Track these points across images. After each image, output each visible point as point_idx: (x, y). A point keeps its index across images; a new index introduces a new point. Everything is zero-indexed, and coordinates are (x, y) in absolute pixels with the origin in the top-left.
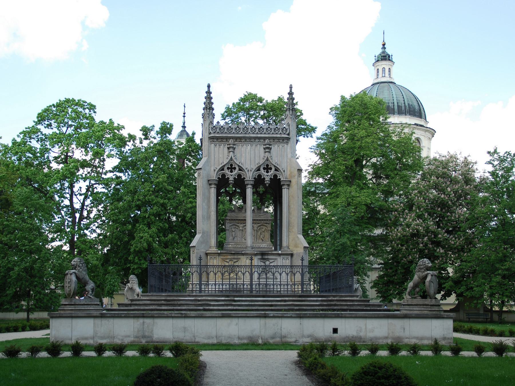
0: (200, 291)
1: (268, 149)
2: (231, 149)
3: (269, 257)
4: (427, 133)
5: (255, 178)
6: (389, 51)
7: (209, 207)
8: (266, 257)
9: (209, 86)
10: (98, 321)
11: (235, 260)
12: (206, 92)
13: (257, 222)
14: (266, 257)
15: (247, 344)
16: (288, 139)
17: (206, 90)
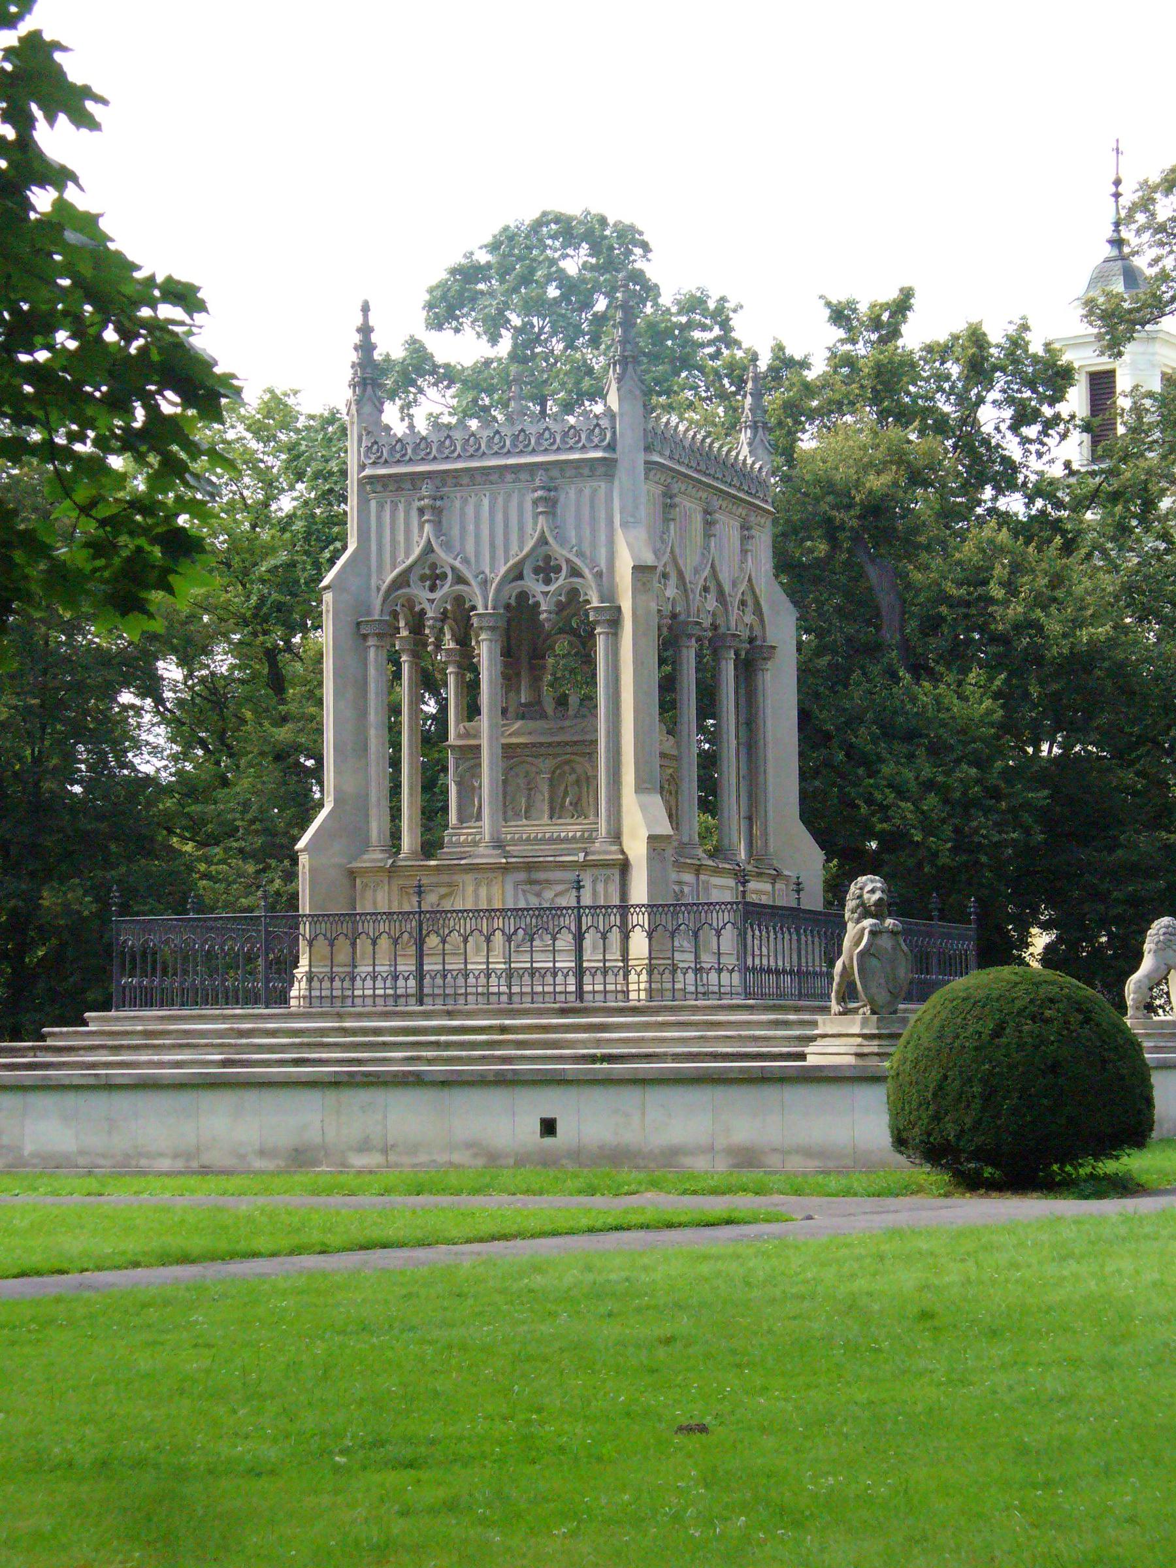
0: (580, 993)
1: (550, 505)
2: (436, 513)
3: (550, 875)
5: (508, 607)
7: (363, 713)
8: (541, 876)
9: (366, 309)
11: (443, 890)
12: (359, 330)
13: (551, 751)
14: (541, 876)
17: (359, 321)
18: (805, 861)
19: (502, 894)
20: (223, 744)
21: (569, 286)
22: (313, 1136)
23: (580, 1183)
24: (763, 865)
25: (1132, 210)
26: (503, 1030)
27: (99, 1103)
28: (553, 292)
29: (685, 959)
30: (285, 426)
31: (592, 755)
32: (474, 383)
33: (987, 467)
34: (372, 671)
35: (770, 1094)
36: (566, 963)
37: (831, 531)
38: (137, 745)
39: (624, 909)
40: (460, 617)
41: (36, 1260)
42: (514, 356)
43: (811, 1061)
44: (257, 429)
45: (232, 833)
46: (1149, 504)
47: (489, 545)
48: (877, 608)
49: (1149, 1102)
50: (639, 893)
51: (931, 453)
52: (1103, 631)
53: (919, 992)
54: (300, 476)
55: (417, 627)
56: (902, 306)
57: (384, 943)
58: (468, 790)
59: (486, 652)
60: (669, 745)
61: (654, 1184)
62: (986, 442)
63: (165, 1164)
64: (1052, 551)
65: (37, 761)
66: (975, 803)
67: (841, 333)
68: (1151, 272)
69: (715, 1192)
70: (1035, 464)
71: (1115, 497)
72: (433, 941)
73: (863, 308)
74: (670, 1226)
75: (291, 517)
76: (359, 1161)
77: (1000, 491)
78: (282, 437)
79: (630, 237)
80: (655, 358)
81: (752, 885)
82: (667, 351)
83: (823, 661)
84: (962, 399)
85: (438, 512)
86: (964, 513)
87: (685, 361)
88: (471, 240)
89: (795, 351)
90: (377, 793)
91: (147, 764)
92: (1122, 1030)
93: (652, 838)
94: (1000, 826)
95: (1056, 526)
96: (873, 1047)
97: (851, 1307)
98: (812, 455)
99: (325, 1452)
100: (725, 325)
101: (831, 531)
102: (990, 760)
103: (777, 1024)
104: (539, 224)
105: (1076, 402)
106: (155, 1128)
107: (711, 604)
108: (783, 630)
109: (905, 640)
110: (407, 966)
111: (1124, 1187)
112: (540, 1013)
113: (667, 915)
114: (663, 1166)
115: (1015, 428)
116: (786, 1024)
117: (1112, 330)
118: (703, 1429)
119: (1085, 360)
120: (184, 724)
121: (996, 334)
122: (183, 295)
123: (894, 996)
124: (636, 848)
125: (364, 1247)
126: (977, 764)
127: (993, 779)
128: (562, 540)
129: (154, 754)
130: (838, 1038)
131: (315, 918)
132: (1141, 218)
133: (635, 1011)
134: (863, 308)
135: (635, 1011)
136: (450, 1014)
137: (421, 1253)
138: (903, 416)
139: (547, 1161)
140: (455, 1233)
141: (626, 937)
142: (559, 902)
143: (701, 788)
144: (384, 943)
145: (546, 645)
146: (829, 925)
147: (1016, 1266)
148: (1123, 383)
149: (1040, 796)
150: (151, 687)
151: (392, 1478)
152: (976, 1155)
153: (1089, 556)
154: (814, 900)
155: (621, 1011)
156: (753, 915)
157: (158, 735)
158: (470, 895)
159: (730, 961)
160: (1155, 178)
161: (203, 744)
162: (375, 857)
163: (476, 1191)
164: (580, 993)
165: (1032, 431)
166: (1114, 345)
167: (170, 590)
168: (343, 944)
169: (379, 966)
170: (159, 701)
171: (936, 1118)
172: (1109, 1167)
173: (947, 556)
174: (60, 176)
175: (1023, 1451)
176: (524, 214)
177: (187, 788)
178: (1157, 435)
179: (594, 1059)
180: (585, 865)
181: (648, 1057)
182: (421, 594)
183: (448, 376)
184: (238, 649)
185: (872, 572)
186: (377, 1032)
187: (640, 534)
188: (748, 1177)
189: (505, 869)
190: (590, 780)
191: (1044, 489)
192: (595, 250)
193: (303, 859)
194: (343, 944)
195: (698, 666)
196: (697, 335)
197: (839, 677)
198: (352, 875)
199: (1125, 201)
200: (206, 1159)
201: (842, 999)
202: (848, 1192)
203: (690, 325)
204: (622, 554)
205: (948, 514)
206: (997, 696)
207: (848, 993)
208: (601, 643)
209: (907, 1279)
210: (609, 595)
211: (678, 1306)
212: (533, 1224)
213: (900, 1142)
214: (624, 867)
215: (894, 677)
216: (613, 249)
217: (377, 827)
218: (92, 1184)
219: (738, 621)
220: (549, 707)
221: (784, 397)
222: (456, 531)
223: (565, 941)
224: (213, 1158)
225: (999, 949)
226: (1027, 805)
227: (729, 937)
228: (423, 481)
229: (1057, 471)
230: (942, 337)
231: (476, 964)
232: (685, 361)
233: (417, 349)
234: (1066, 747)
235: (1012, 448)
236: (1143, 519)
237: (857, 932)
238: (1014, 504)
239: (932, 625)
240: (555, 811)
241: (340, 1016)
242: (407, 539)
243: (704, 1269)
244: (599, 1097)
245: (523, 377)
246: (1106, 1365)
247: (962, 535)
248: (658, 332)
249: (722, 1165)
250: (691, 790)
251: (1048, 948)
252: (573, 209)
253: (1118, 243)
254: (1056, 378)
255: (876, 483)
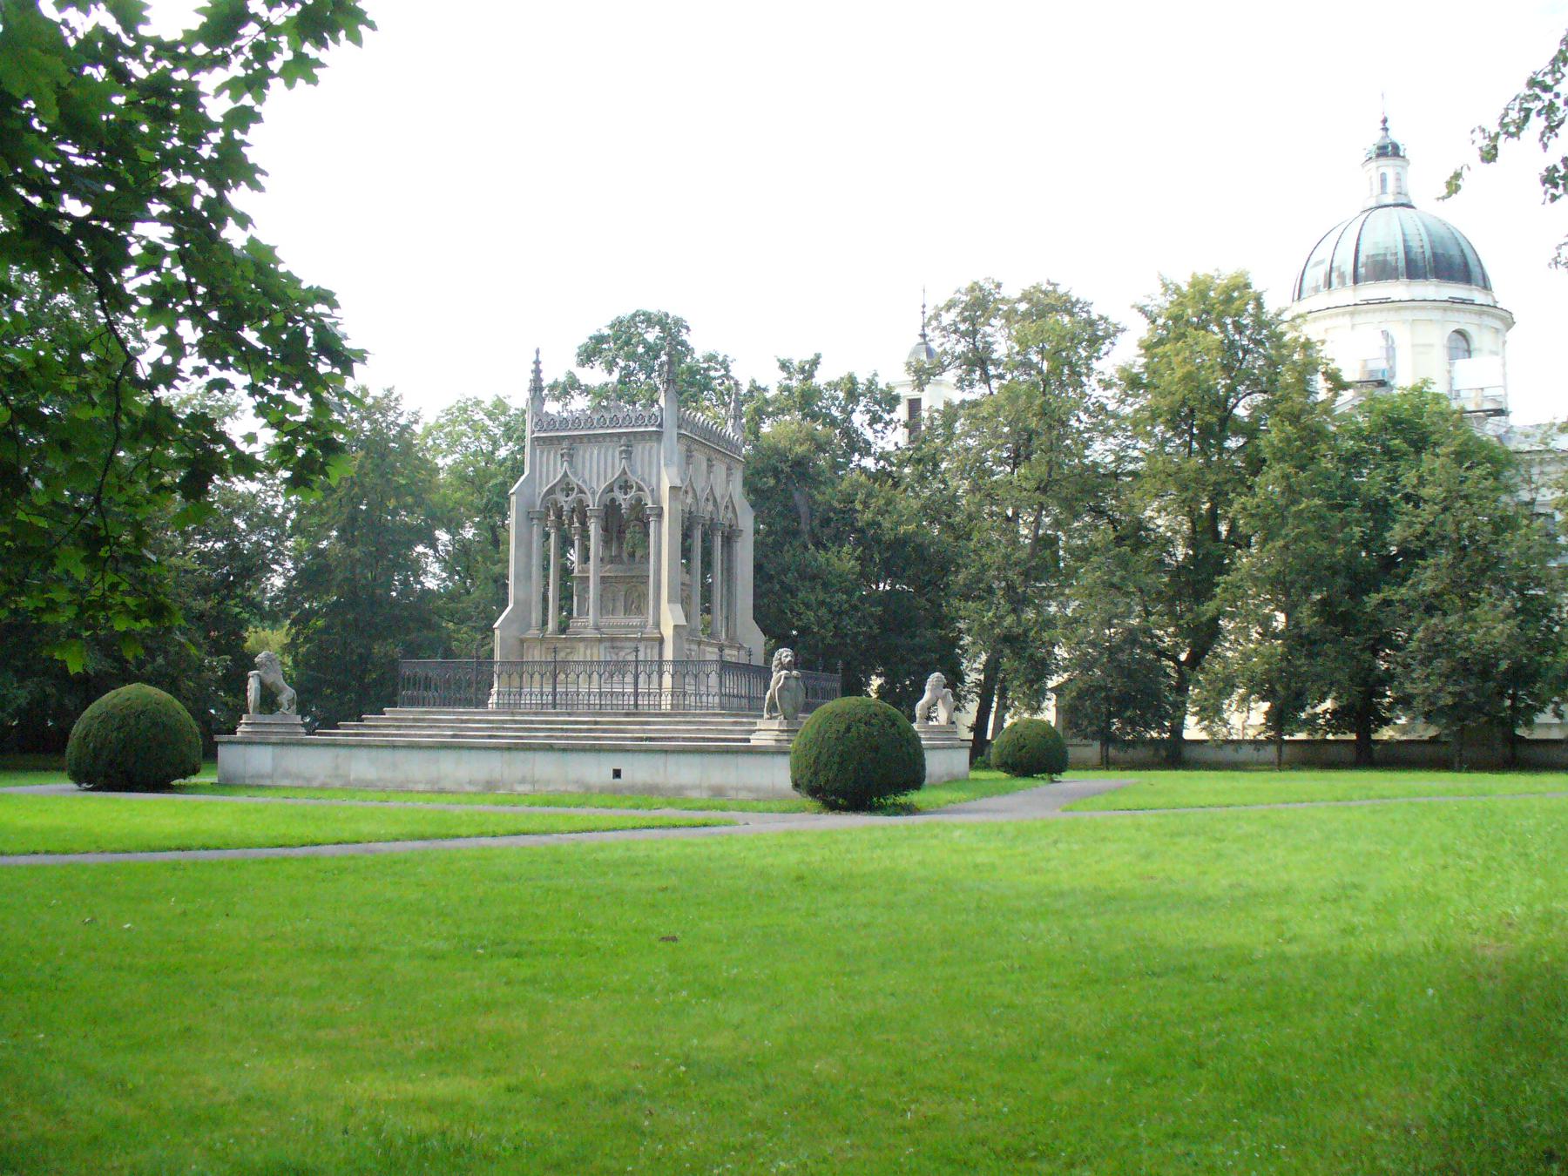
0: (636, 705)
1: (628, 454)
2: (570, 457)
4: (1485, 318)
6: (1395, 136)
7: (529, 557)
9: (538, 352)
10: (278, 750)
14: (618, 644)
15: (219, 784)
16: (659, 435)
18: (754, 639)
19: (599, 653)
20: (468, 572)
21: (649, 348)
22: (496, 775)
23: (628, 803)
24: (733, 642)
25: (930, 319)
26: (596, 723)
27: (386, 755)
28: (641, 350)
29: (690, 689)
30: (504, 413)
31: (646, 583)
32: (599, 393)
33: (857, 445)
34: (535, 538)
35: (730, 758)
36: (629, 689)
37: (776, 473)
38: (425, 573)
39: (661, 663)
40: (581, 511)
41: (346, 836)
42: (620, 381)
43: (753, 743)
44: (490, 415)
45: (470, 618)
46: (936, 465)
47: (596, 473)
48: (798, 513)
49: (923, 767)
50: (668, 654)
51: (828, 436)
52: (912, 527)
53: (808, 708)
54: (510, 439)
55: (559, 515)
56: (815, 363)
57: (537, 677)
58: (583, 600)
59: (593, 528)
60: (687, 578)
61: (671, 805)
62: (856, 431)
63: (421, 787)
64: (887, 487)
65: (374, 579)
66: (847, 613)
67: (785, 375)
68: (939, 350)
69: (701, 809)
70: (881, 443)
71: (919, 461)
72: (562, 677)
73: (796, 363)
74: (675, 826)
75: (505, 459)
76: (520, 788)
77: (862, 456)
78: (502, 419)
79: (679, 323)
80: (691, 385)
81: (727, 651)
82: (690, 381)
83: (770, 540)
84: (844, 410)
85: (571, 456)
86: (844, 466)
87: (706, 387)
88: (601, 324)
89: (761, 383)
90: (536, 598)
91: (431, 583)
92: (911, 730)
93: (676, 627)
94: (858, 625)
95: (890, 474)
96: (785, 736)
97: (762, 874)
98: (768, 435)
99: (471, 948)
100: (727, 369)
101: (776, 473)
102: (854, 590)
103: (735, 723)
104: (635, 316)
105: (901, 412)
106: (416, 767)
107: (710, 507)
108: (746, 521)
109: (812, 530)
110: (548, 689)
111: (909, 810)
112: (616, 715)
113: (683, 667)
114: (675, 796)
115: (870, 425)
116: (741, 724)
117: (919, 378)
118: (674, 939)
119: (906, 392)
120: (448, 566)
121: (862, 379)
122: (326, 297)
123: (796, 711)
124: (668, 632)
125: (516, 834)
126: (846, 592)
127: (854, 601)
128: (633, 472)
129: (433, 578)
130: (766, 731)
131: (502, 663)
132: (934, 323)
133: (664, 715)
134: (796, 363)
135: (664, 715)
136: (569, 715)
137: (544, 838)
138: (814, 417)
139: (616, 791)
140: (564, 828)
141: (661, 677)
142: (627, 657)
143: (702, 599)
144: (537, 677)
145: (624, 525)
146: (764, 673)
147: (848, 851)
148: (925, 405)
149: (878, 610)
150: (432, 543)
151: (505, 963)
152: (836, 792)
153: (905, 490)
154: (758, 660)
155: (657, 715)
156: (725, 667)
157: (435, 568)
158: (582, 653)
159: (715, 690)
160: (942, 304)
161: (458, 573)
162: (534, 632)
163: (577, 806)
164: (636, 705)
165: (879, 426)
166: (920, 386)
167: (326, 475)
168: (516, 678)
169: (536, 690)
170: (436, 551)
171: (816, 774)
172: (902, 799)
173: (834, 487)
174: (244, 221)
175: (840, 954)
176: (626, 312)
177: (452, 596)
178: (940, 431)
179: (641, 739)
180: (641, 639)
181: (669, 739)
182: (561, 498)
183: (587, 390)
184: (477, 526)
185: (797, 495)
186: (532, 722)
187: (674, 470)
188: (719, 802)
189: (600, 640)
190: (645, 595)
191: (884, 456)
192: (663, 330)
193: (497, 632)
194: (516, 678)
195: (702, 539)
196: (712, 373)
197: (778, 547)
198: (522, 641)
199: (927, 315)
200: (441, 785)
201: (769, 711)
202: (769, 811)
203: (708, 369)
204: (663, 477)
205: (836, 466)
206: (857, 559)
207: (773, 708)
208: (652, 525)
209: (793, 858)
210: (657, 501)
211: (672, 870)
212: (602, 824)
213: (796, 785)
214: (661, 641)
215: (806, 548)
216: (672, 329)
217: (536, 616)
218: (384, 796)
219: (724, 517)
220: (625, 556)
221: (756, 406)
222: (580, 466)
223: (629, 679)
224: (448, 785)
225: (854, 687)
226: (871, 615)
227: (714, 680)
228: (563, 440)
229: (891, 448)
230: (836, 379)
231: (583, 689)
232: (706, 387)
233: (571, 376)
234: (893, 586)
235: (869, 434)
236: (933, 473)
237: (778, 677)
238: (869, 463)
239: (826, 522)
240: (627, 611)
241: (513, 714)
242: (553, 469)
243: (688, 850)
244: (642, 759)
245: (625, 390)
246: (890, 906)
247: (842, 478)
248: (692, 371)
249: (705, 795)
250: (697, 599)
251: (880, 686)
252: (652, 308)
253: (924, 336)
254: (891, 400)
255: (799, 450)
